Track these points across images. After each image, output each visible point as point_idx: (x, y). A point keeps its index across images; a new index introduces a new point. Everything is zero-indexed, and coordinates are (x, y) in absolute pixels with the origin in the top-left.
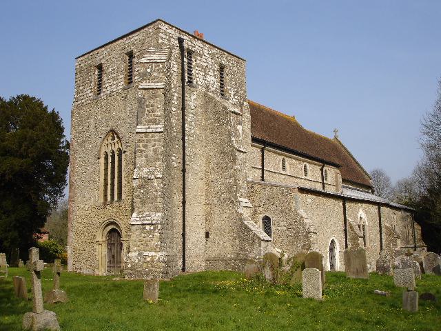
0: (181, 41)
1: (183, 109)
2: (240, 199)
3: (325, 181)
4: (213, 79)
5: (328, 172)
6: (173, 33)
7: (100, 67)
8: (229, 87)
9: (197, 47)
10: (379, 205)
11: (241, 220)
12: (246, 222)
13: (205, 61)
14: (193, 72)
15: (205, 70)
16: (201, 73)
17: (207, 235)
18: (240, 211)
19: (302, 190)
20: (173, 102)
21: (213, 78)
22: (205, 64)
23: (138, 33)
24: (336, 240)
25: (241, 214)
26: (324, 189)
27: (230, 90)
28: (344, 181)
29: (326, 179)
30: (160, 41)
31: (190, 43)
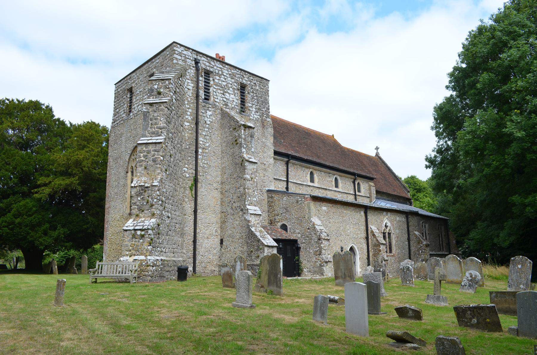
0: (197, 62)
1: (197, 124)
2: (248, 207)
3: (357, 193)
4: (234, 98)
5: (361, 183)
6: (190, 54)
7: (131, 90)
8: (250, 105)
9: (215, 67)
10: (407, 214)
11: (248, 227)
12: (253, 229)
13: (224, 80)
14: (211, 90)
15: (224, 90)
16: (219, 91)
17: (222, 241)
18: (248, 218)
19: (316, 199)
20: (187, 117)
21: (232, 96)
22: (224, 84)
23: (159, 56)
24: (356, 247)
25: (249, 221)
26: (356, 200)
27: (252, 107)
28: (378, 192)
29: (359, 191)
30: (175, 61)
31: (207, 64)
